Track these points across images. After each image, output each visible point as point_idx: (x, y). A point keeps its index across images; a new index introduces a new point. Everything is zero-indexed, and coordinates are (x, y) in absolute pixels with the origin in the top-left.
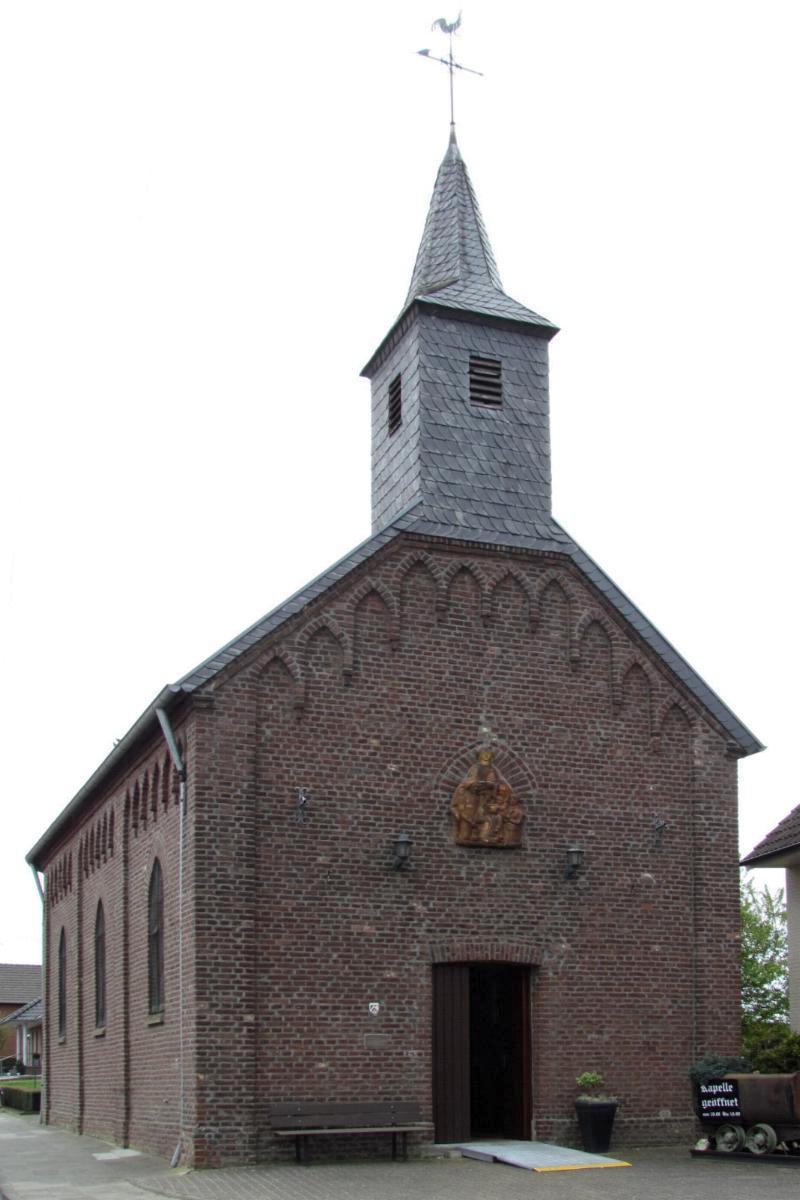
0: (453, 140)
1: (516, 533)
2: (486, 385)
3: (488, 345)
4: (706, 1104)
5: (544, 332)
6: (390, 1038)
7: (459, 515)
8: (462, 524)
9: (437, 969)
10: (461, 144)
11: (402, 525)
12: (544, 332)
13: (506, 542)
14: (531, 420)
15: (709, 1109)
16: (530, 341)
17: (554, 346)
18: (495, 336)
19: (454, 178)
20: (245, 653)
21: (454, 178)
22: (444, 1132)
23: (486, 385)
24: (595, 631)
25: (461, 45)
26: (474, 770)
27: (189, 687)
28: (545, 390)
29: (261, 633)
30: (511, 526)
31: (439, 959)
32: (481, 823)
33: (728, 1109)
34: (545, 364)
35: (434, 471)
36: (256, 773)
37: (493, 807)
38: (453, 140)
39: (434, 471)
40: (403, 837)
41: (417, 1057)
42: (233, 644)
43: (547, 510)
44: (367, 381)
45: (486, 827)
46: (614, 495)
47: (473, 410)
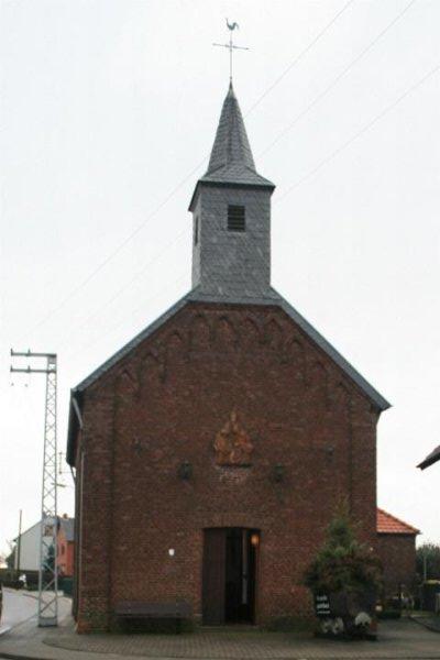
0: (231, 87)
1: (250, 296)
2: (236, 218)
3: (238, 199)
4: (319, 606)
5: (270, 189)
6: (177, 569)
7: (220, 290)
8: (221, 293)
9: (207, 531)
10: (235, 89)
11: (189, 298)
12: (270, 189)
13: (244, 301)
14: (261, 235)
15: (321, 609)
16: (262, 193)
17: (274, 198)
18: (242, 193)
19: (231, 105)
20: (109, 370)
21: (231, 105)
22: (208, 620)
23: (236, 218)
24: (295, 345)
25: (225, 36)
26: (227, 425)
27: (81, 389)
28: (269, 219)
29: (159, 325)
30: (248, 293)
31: (207, 526)
32: (229, 453)
33: (325, 610)
34: (269, 205)
35: (207, 269)
36: (114, 431)
37: (236, 444)
38: (231, 87)
39: (207, 269)
40: (187, 462)
41: (195, 577)
42: (102, 366)
43: (268, 283)
44: (190, 213)
45: (232, 454)
46: (307, 274)
47: (229, 234)
